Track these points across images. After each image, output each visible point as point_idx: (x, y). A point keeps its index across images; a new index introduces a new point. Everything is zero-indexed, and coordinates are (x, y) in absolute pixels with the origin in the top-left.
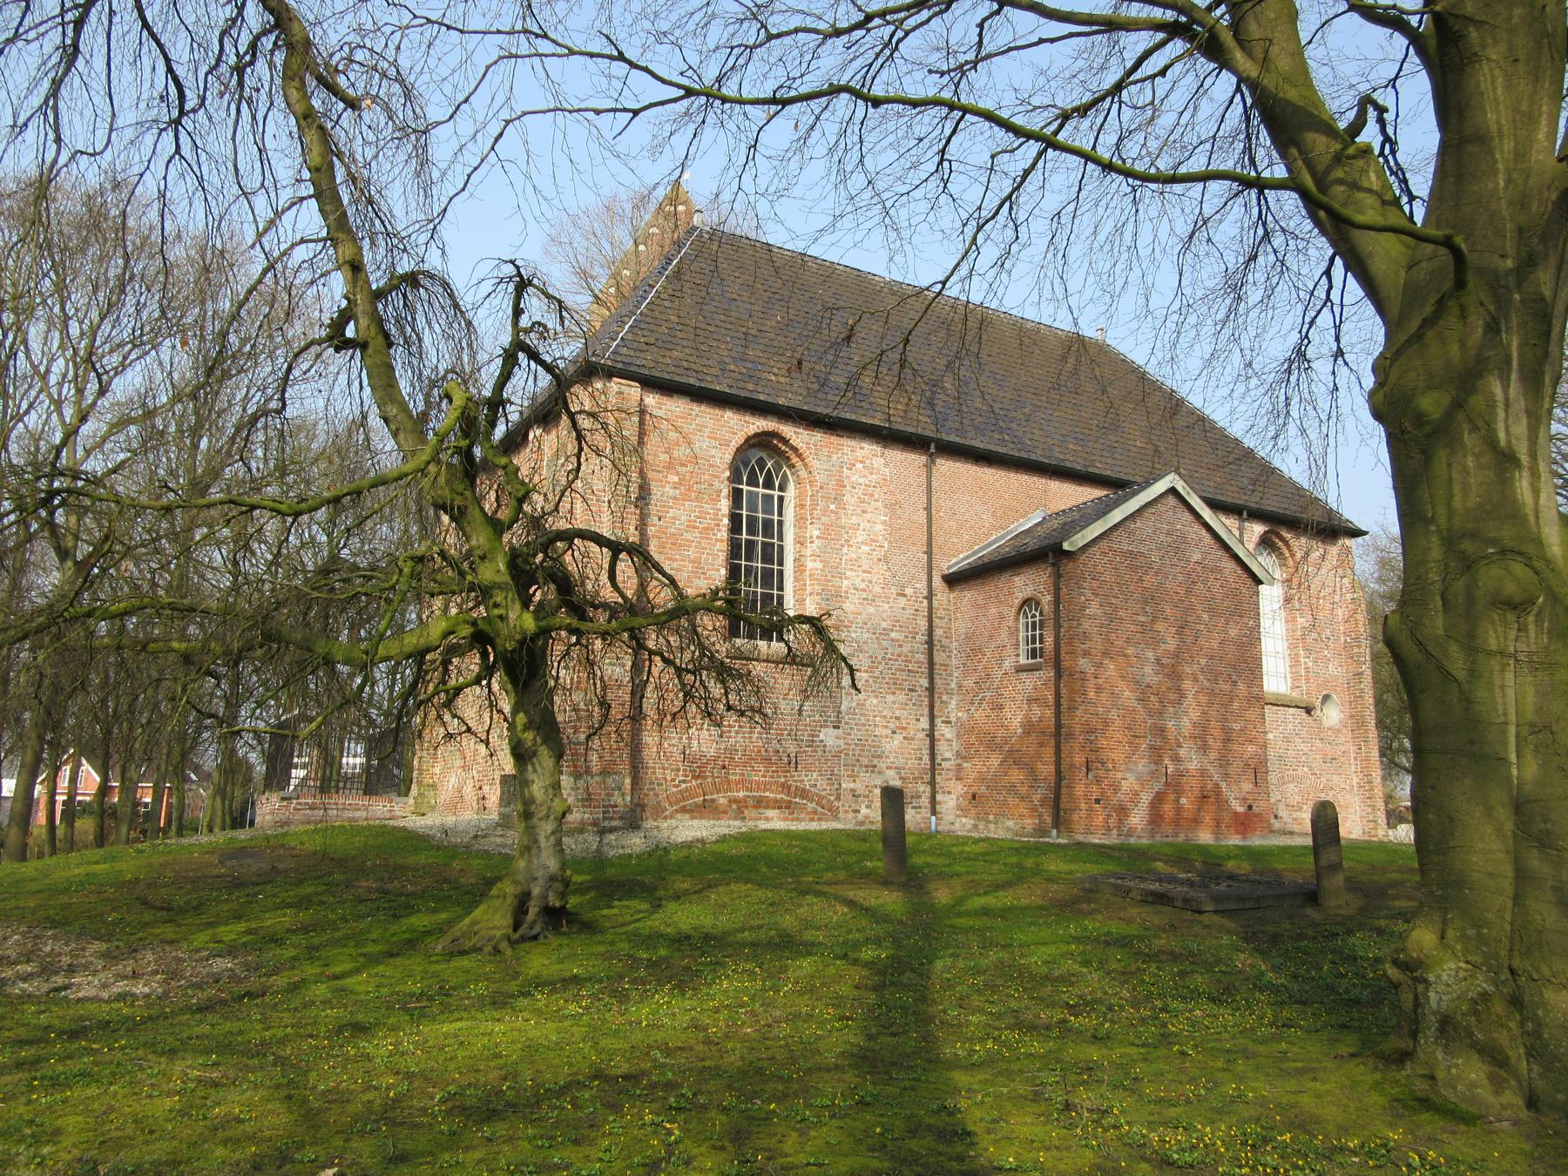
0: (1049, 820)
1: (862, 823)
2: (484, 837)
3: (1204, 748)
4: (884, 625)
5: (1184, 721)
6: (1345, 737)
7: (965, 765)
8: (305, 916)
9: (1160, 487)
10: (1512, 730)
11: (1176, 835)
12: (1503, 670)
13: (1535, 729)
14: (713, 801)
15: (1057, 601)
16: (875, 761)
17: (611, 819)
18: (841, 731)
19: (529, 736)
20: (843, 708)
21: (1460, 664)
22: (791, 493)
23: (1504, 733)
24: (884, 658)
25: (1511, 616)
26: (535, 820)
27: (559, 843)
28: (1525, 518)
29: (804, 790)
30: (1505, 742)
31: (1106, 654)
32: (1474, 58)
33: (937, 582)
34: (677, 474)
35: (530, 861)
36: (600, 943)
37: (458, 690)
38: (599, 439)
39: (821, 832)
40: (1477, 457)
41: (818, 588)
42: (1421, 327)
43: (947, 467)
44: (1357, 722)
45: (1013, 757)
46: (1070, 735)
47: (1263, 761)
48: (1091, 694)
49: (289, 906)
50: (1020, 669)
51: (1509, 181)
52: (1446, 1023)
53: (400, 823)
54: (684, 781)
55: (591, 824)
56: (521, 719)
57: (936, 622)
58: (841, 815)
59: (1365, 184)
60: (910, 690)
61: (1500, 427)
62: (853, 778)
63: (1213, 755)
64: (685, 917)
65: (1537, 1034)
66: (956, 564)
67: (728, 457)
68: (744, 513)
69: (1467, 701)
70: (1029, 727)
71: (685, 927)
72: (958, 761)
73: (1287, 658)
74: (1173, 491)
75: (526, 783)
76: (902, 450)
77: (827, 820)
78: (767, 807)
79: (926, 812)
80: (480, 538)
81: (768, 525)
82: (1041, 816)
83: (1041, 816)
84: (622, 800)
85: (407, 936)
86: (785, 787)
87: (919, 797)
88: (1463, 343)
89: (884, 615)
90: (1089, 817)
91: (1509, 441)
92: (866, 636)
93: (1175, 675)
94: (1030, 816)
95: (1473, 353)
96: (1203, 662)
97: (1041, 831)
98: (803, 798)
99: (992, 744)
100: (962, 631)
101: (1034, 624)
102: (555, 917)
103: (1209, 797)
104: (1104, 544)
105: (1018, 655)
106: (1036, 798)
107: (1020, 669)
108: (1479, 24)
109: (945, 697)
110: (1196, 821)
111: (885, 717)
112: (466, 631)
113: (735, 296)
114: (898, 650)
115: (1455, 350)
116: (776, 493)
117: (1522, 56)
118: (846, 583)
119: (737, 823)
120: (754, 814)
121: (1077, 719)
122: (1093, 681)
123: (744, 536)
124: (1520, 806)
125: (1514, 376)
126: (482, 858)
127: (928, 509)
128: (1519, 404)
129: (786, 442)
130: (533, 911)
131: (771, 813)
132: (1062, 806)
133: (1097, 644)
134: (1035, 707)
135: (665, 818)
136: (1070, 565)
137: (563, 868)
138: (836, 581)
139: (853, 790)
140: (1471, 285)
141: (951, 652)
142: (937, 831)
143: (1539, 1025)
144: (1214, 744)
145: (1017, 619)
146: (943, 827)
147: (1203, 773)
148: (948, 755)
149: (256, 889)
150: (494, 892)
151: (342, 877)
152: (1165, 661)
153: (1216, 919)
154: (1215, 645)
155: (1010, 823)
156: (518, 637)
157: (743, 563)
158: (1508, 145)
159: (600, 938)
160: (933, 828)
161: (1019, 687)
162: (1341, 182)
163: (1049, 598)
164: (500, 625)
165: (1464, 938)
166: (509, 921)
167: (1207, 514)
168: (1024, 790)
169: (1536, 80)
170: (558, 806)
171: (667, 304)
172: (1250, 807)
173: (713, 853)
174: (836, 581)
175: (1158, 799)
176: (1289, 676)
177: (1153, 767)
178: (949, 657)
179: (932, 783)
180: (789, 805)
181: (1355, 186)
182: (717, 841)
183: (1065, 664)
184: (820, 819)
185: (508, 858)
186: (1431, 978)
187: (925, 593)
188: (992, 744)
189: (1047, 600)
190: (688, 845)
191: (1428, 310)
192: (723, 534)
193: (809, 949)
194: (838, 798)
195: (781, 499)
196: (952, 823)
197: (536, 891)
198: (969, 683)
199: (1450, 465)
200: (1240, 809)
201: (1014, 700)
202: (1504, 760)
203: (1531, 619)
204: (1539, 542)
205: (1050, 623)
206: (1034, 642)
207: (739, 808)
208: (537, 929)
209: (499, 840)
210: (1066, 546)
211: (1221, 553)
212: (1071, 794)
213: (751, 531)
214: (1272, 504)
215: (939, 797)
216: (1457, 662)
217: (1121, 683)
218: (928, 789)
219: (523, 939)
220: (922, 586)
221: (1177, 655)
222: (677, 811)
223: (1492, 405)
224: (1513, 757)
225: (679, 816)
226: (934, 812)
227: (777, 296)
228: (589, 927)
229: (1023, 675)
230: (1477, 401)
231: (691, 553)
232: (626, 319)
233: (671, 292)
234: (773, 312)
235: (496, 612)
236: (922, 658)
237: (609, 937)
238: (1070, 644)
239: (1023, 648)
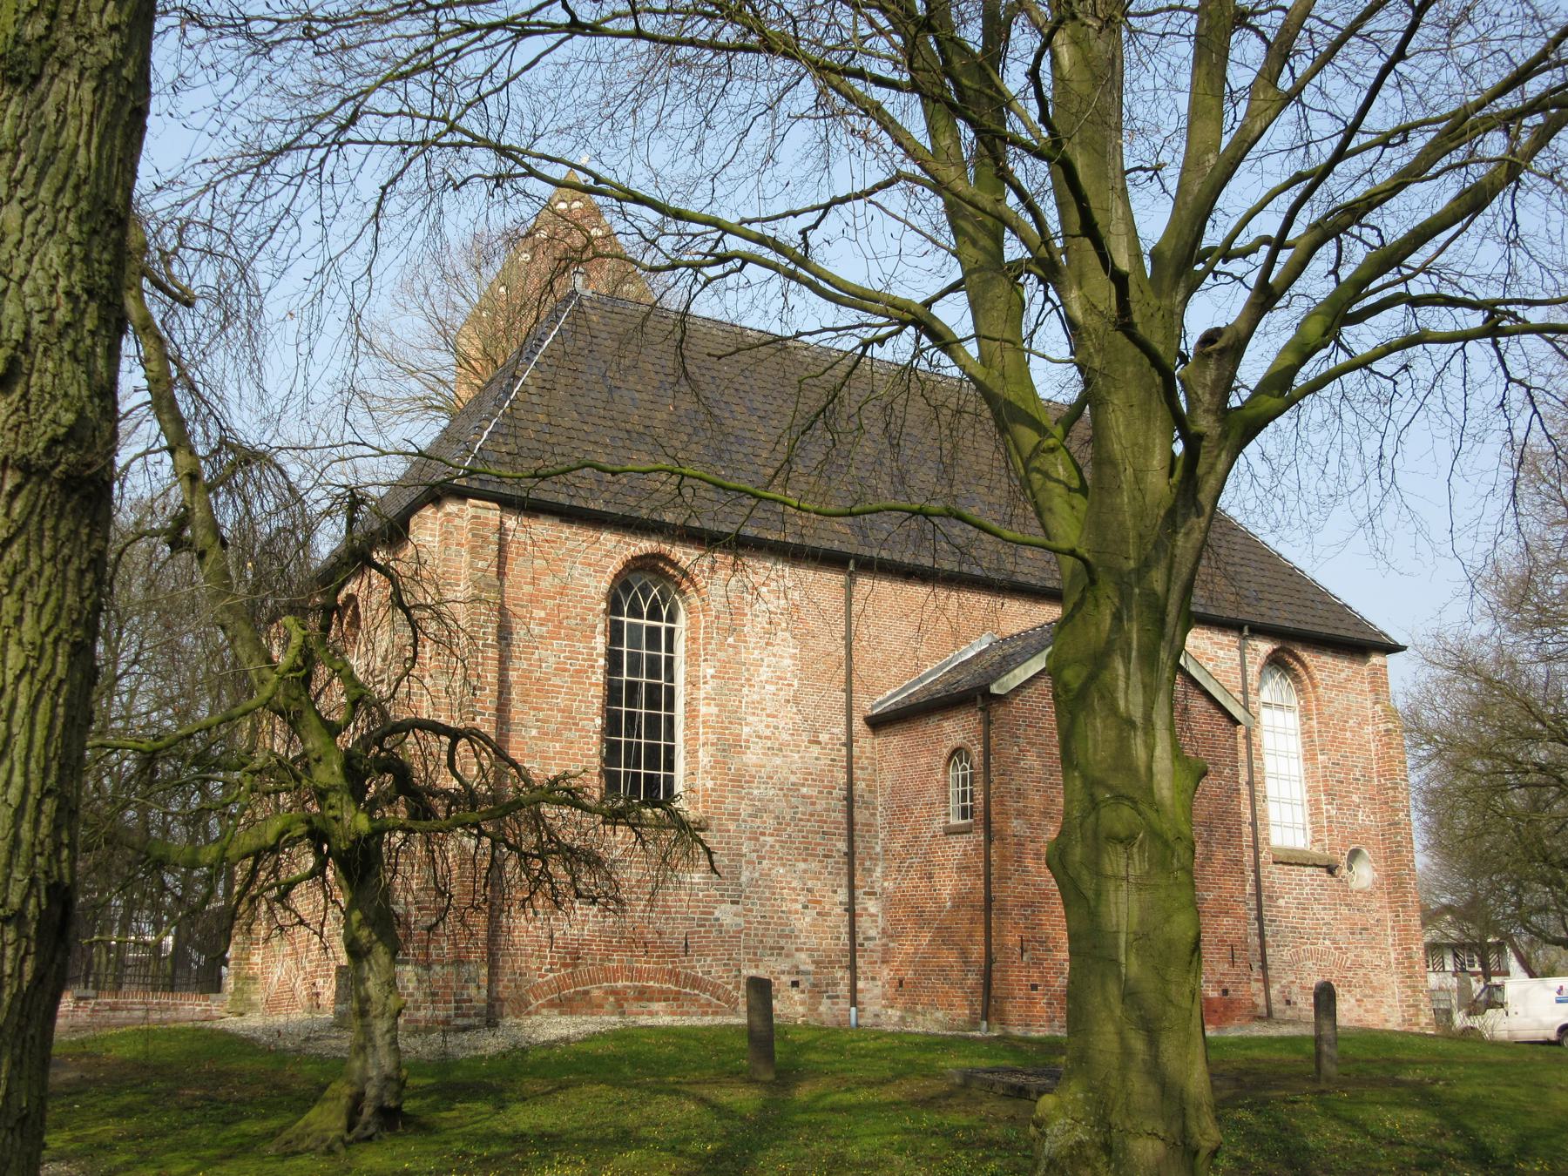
2: (317, 1039)
4: (793, 779)
8: (130, 1124)
12: (1117, 889)
14: (586, 993)
15: (987, 753)
16: (782, 942)
18: (740, 907)
19: (364, 934)
20: (743, 879)
22: (681, 624)
23: (1116, 939)
24: (793, 819)
25: (1120, 848)
26: (370, 1018)
27: (394, 1041)
28: (1137, 770)
29: (695, 979)
33: (859, 724)
34: (544, 609)
36: (436, 1142)
37: (291, 885)
38: (432, 627)
39: (708, 1028)
41: (712, 738)
43: (864, 584)
45: (944, 935)
46: (1003, 910)
49: (111, 1115)
50: (950, 831)
53: (219, 1025)
56: (356, 916)
57: (858, 773)
59: (1055, 475)
60: (826, 856)
61: (1121, 696)
62: (756, 962)
64: (524, 1117)
66: (881, 703)
67: (605, 586)
68: (625, 649)
70: (960, 901)
71: (523, 1127)
73: (1306, 805)
75: (362, 981)
77: (724, 1014)
78: (650, 1000)
79: (843, 1004)
80: (315, 742)
81: (653, 663)
84: (477, 994)
85: (238, 1141)
86: (673, 975)
87: (836, 984)
89: (794, 767)
91: (1127, 707)
92: (772, 792)
97: (974, 1024)
98: (694, 987)
99: (920, 918)
100: (888, 783)
102: (392, 1119)
105: (948, 814)
107: (950, 831)
109: (868, 864)
111: (794, 889)
112: (301, 829)
114: (810, 809)
116: (663, 625)
118: (746, 729)
119: (615, 1019)
120: (635, 1007)
123: (625, 677)
126: (315, 1062)
128: (1136, 678)
129: (674, 565)
130: (368, 1111)
131: (657, 1006)
132: (993, 993)
134: (964, 876)
135: (529, 1014)
136: (1001, 711)
137: (398, 1067)
138: (736, 729)
141: (875, 808)
142: (858, 1025)
145: (946, 772)
146: (867, 1020)
148: (872, 933)
149: (71, 1099)
150: (328, 1093)
151: (161, 1085)
155: (939, 1015)
156: (352, 837)
157: (624, 709)
159: (435, 1138)
160: (853, 1021)
163: (979, 748)
164: (335, 826)
166: (342, 1122)
169: (1148, 420)
170: (393, 1003)
171: (535, 399)
172: (1225, 992)
173: (577, 1053)
174: (736, 729)
176: (1308, 826)
178: (874, 815)
179: (853, 967)
180: (677, 997)
181: (1047, 476)
182: (584, 1040)
184: (715, 1013)
185: (344, 1061)
187: (844, 739)
188: (920, 918)
189: (977, 750)
190: (550, 1045)
192: (599, 677)
193: (640, 1143)
195: (670, 632)
196: (877, 1016)
197: (371, 1091)
198: (897, 846)
201: (943, 867)
203: (1135, 850)
204: (1149, 790)
205: (980, 778)
206: (964, 800)
207: (617, 1000)
208: (372, 1130)
209: (334, 1043)
210: (994, 689)
213: (634, 669)
214: (1283, 618)
218: (848, 975)
219: (358, 1140)
220: (840, 730)
222: (543, 1006)
224: (1123, 959)
225: (545, 1011)
226: (854, 1002)
228: (424, 1128)
229: (952, 839)
230: (1106, 676)
231: (561, 701)
232: (485, 423)
233: (541, 384)
235: (331, 813)
236: (840, 817)
237: (444, 1137)
238: (1002, 803)
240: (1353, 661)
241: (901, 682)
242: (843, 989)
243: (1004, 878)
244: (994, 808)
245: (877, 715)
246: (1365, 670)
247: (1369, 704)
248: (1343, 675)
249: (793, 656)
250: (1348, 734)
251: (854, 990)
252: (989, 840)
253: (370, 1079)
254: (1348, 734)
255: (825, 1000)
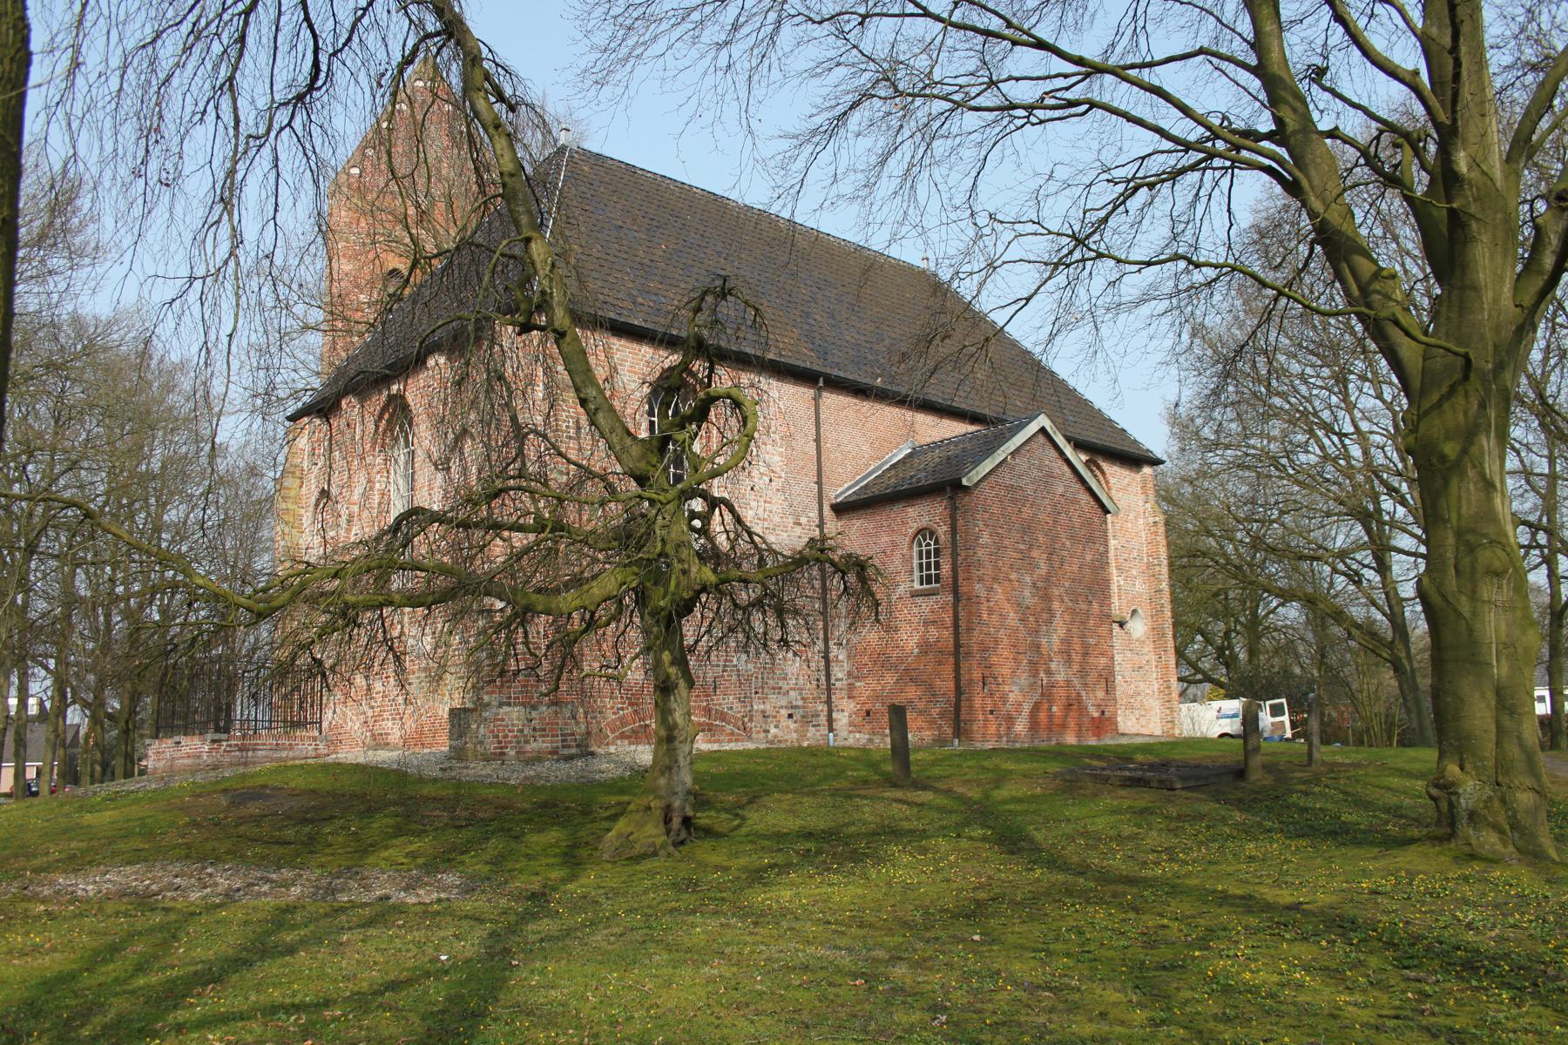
0: (949, 731)
1: (772, 742)
3: (1068, 662)
5: (1053, 639)
6: (1149, 647)
7: (858, 684)
9: (1033, 427)
10: (1494, 646)
11: (1049, 739)
13: (1506, 646)
15: (954, 530)
17: (569, 747)
21: (1467, 608)
23: (1490, 648)
25: (1495, 580)
26: (676, 743)
29: (722, 713)
30: (1491, 654)
31: (995, 579)
32: (1474, 239)
35: (670, 779)
40: (1475, 484)
42: (1440, 400)
44: (1157, 632)
46: (968, 654)
47: (1112, 673)
48: (985, 616)
51: (1490, 315)
52: (1473, 816)
54: (622, 709)
55: (551, 753)
58: (754, 736)
62: (764, 700)
63: (1076, 667)
65: (1514, 816)
69: (1470, 630)
70: (925, 647)
72: (851, 681)
74: (1043, 430)
76: (794, 384)
79: (824, 730)
82: (940, 728)
83: (940, 728)
87: (818, 716)
88: (1466, 413)
90: (985, 726)
93: (1046, 598)
94: (929, 729)
95: (1471, 420)
96: (1067, 584)
98: (723, 721)
101: (928, 552)
103: (1074, 704)
104: (992, 479)
106: (935, 712)
107: (915, 594)
108: (1478, 220)
110: (1064, 726)
113: (620, 223)
115: (1461, 416)
117: (1500, 242)
121: (974, 640)
122: (986, 604)
124: (1499, 692)
125: (1492, 435)
127: (818, 440)
128: (1496, 452)
133: (988, 571)
139: (763, 712)
140: (1472, 379)
143: (1515, 812)
144: (1076, 658)
146: (840, 743)
147: (1068, 682)
148: (840, 675)
152: (1040, 584)
153: (1184, 793)
154: (1075, 568)
158: (1490, 294)
161: (915, 610)
162: (1378, 292)
163: (945, 528)
165: (1476, 768)
166: (662, 829)
167: (1068, 451)
168: (921, 705)
172: (1103, 712)
175: (1036, 708)
177: (1032, 680)
179: (829, 702)
181: (1388, 297)
183: (963, 590)
184: (737, 740)
186: (1461, 791)
189: (942, 530)
191: (1444, 390)
194: (751, 720)
197: (677, 804)
199: (1459, 488)
200: (1096, 715)
202: (1490, 664)
205: (946, 553)
206: (929, 568)
211: (1078, 486)
212: (971, 707)
215: (835, 715)
216: (1465, 607)
217: (1007, 606)
218: (826, 708)
220: (814, 514)
221: (1047, 579)
222: (617, 738)
223: (1482, 453)
224: (1495, 663)
225: (619, 742)
226: (831, 729)
227: (655, 223)
229: (919, 600)
230: (1474, 450)
234: (657, 240)
239: (916, 574)
240: (1131, 470)
241: (854, 477)
242: (823, 719)
243: (970, 629)
244: (961, 576)
245: (841, 503)
246: (1138, 477)
247: (1141, 503)
248: (1126, 481)
249: (781, 454)
250: (1129, 525)
251: (830, 720)
252: (957, 599)
253: (676, 793)
254: (1129, 525)
255: (811, 728)
